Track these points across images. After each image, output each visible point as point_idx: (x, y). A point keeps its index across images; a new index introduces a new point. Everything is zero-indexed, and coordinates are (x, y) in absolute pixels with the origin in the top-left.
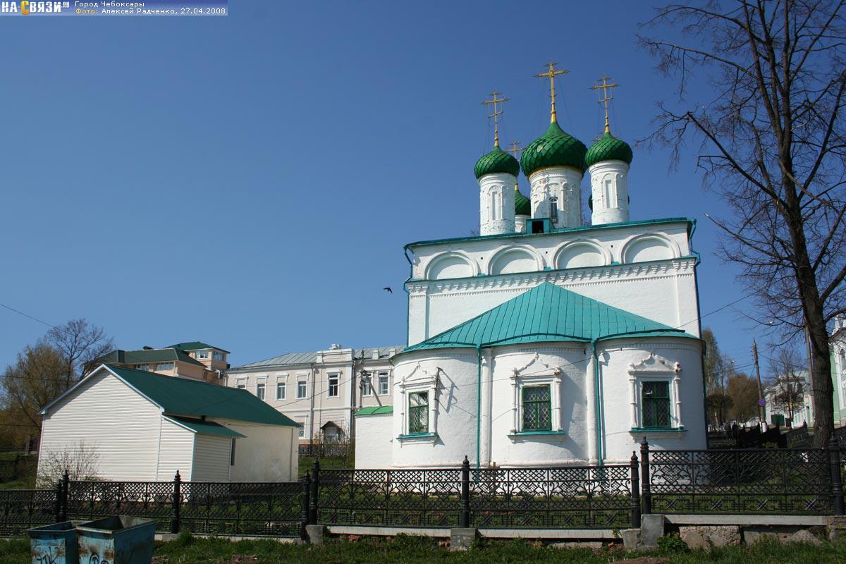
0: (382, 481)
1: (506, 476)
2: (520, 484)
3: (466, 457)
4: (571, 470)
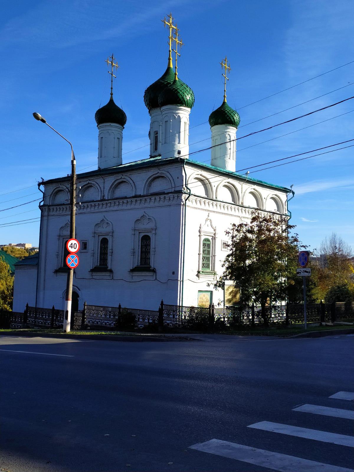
3: (162, 300)
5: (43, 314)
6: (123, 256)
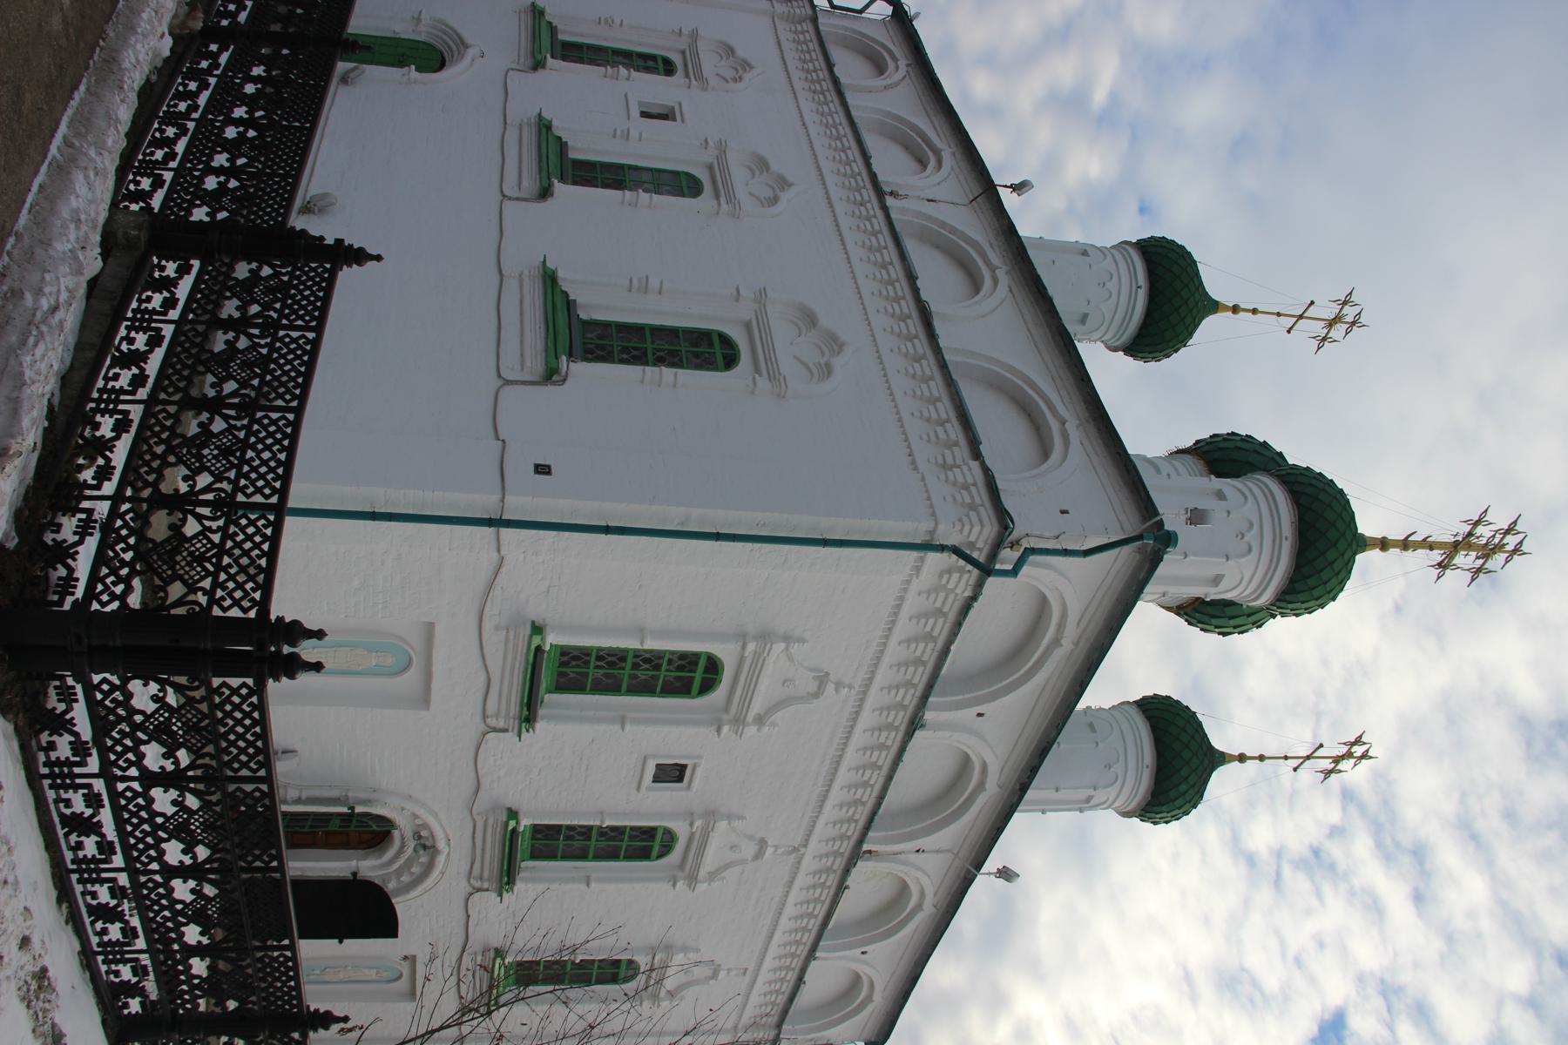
3: (378, 258)
5: (225, 452)
6: (621, 257)
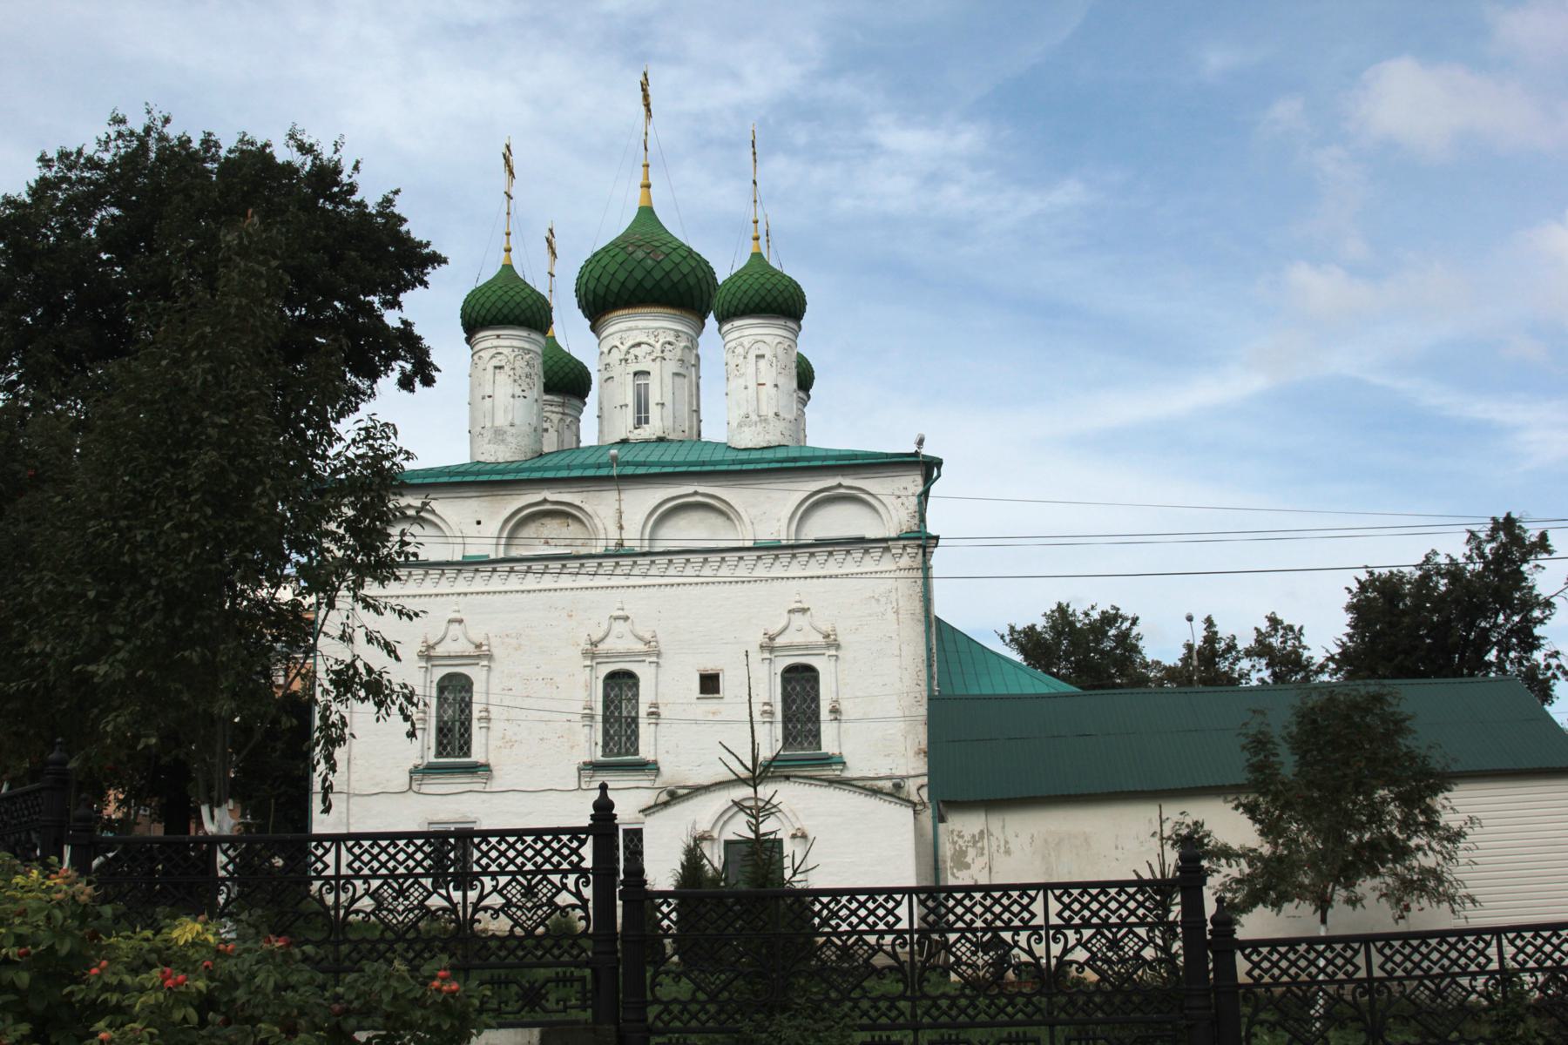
0: (890, 929)
1: (1037, 907)
2: (503, 880)
4: (1405, 943)
